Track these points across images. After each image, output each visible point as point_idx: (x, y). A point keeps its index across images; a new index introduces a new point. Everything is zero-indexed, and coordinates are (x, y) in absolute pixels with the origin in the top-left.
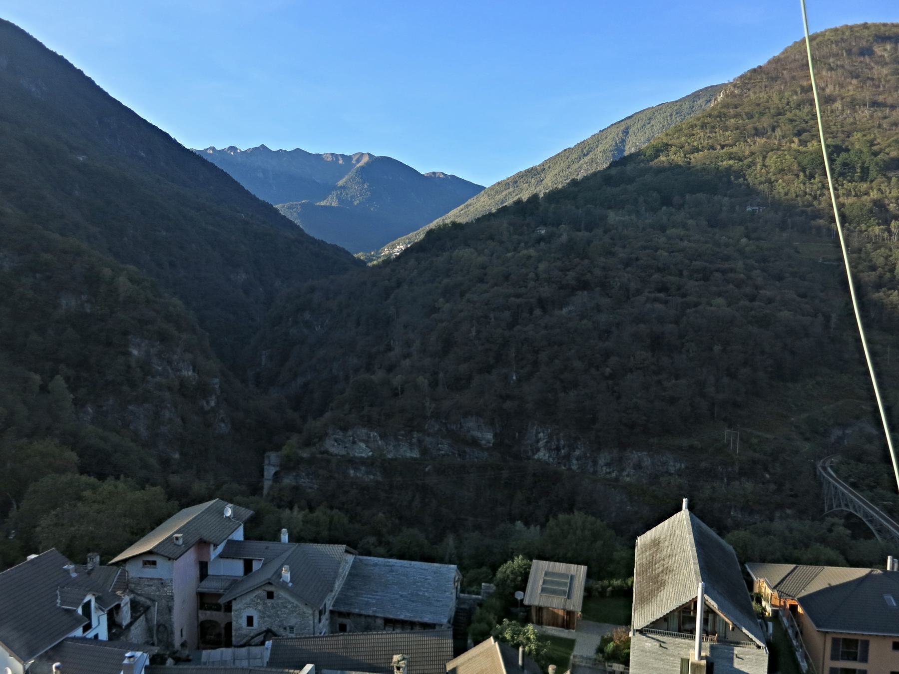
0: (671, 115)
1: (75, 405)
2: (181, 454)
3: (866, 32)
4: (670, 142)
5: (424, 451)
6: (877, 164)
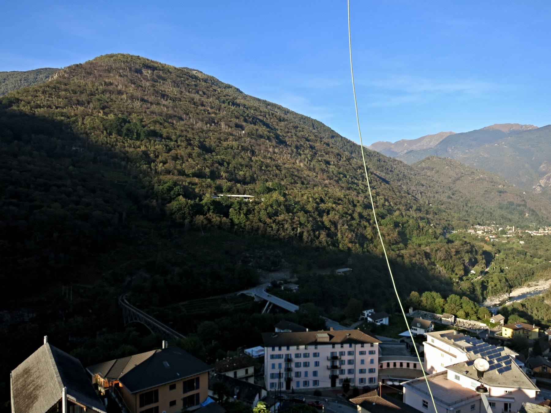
0: (21, 80)
3: (139, 61)
4: (20, 98)
6: (144, 132)
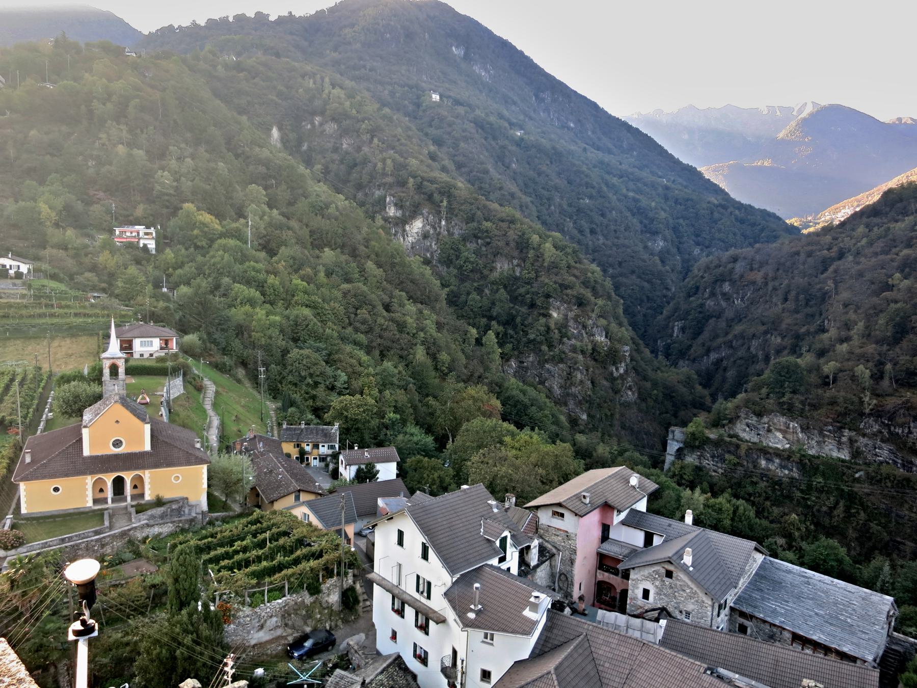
1: (502, 358)
2: (589, 416)
5: (856, 454)
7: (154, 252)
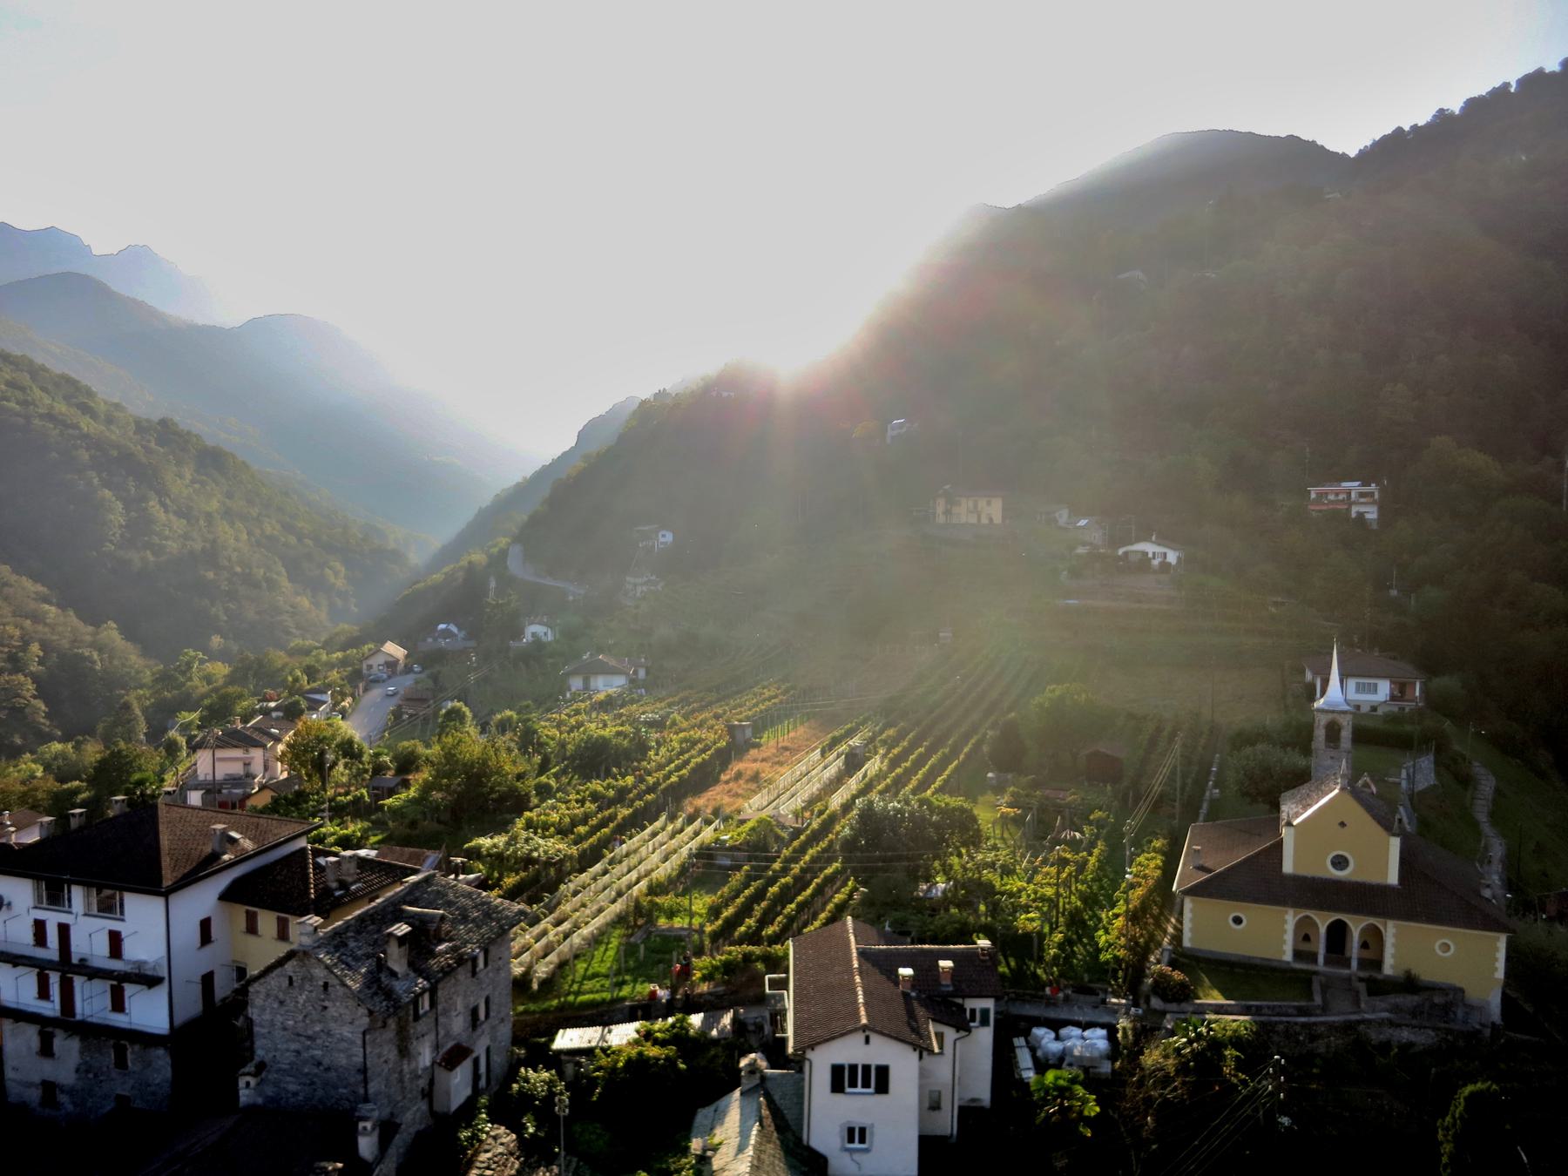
7: (1375, 527)
